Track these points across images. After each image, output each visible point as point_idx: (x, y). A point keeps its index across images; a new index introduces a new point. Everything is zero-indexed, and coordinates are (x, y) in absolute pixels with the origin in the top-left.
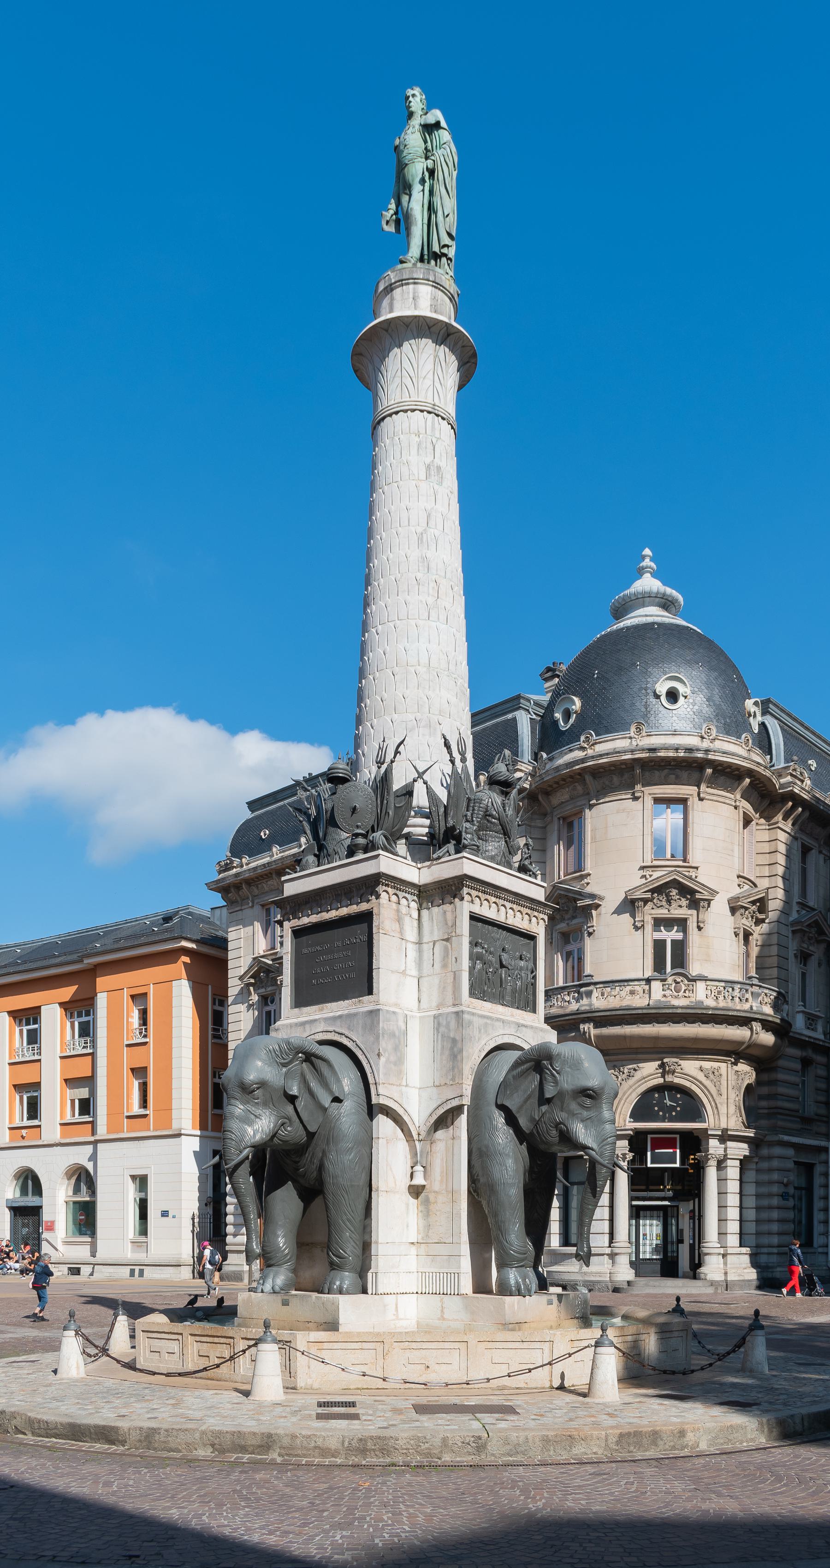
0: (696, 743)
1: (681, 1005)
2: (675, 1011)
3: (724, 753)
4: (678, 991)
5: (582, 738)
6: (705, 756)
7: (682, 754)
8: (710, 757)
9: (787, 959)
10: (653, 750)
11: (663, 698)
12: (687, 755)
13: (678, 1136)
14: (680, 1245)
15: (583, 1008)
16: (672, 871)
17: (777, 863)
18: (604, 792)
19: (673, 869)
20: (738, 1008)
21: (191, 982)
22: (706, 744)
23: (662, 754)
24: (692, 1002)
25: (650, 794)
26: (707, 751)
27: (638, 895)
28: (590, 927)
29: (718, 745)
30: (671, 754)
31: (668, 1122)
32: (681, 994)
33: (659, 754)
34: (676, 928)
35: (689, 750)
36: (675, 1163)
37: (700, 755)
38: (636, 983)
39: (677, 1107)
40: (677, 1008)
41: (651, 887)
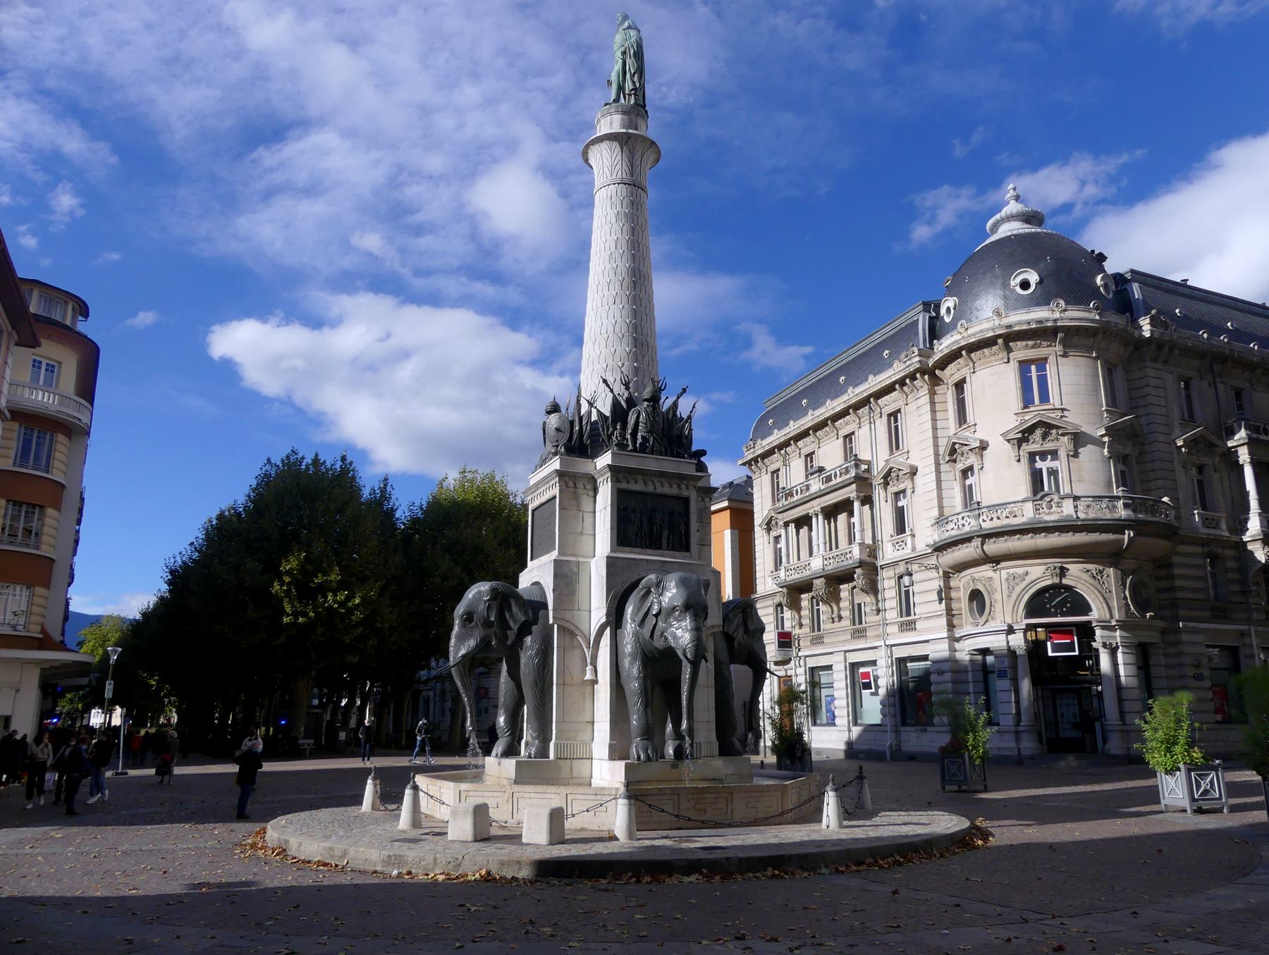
0: (1047, 316)
1: (1052, 519)
2: (1047, 525)
3: (1071, 319)
4: (1051, 508)
5: (959, 326)
6: (1054, 324)
7: (1034, 326)
8: (1059, 324)
9: (1174, 471)
10: (1010, 327)
11: (1018, 290)
12: (1039, 326)
13: (1074, 629)
14: (595, 686)
15: (973, 529)
16: (1037, 415)
17: (1150, 395)
18: (68, 608)
19: (1037, 413)
20: (1108, 517)
21: (737, 532)
22: (1057, 315)
23: (1017, 328)
24: (1062, 516)
25: (1014, 359)
26: (1055, 320)
27: (1011, 436)
28: (1043, 455)
29: (1068, 314)
30: (1025, 327)
31: (1061, 617)
32: (1052, 510)
33: (1015, 329)
34: (1049, 457)
35: (1040, 322)
36: (1075, 651)
37: (1050, 324)
38: (1013, 505)
39: (1050, 605)
40: (1048, 522)
41: (1021, 429)
